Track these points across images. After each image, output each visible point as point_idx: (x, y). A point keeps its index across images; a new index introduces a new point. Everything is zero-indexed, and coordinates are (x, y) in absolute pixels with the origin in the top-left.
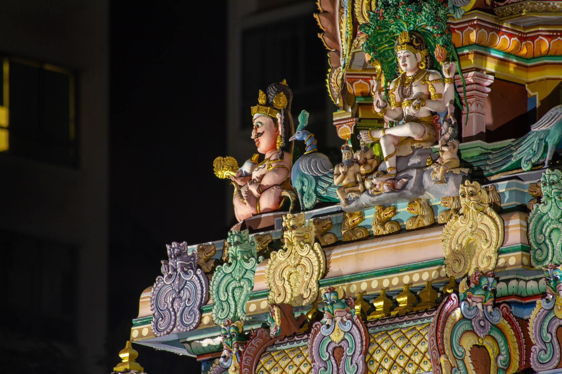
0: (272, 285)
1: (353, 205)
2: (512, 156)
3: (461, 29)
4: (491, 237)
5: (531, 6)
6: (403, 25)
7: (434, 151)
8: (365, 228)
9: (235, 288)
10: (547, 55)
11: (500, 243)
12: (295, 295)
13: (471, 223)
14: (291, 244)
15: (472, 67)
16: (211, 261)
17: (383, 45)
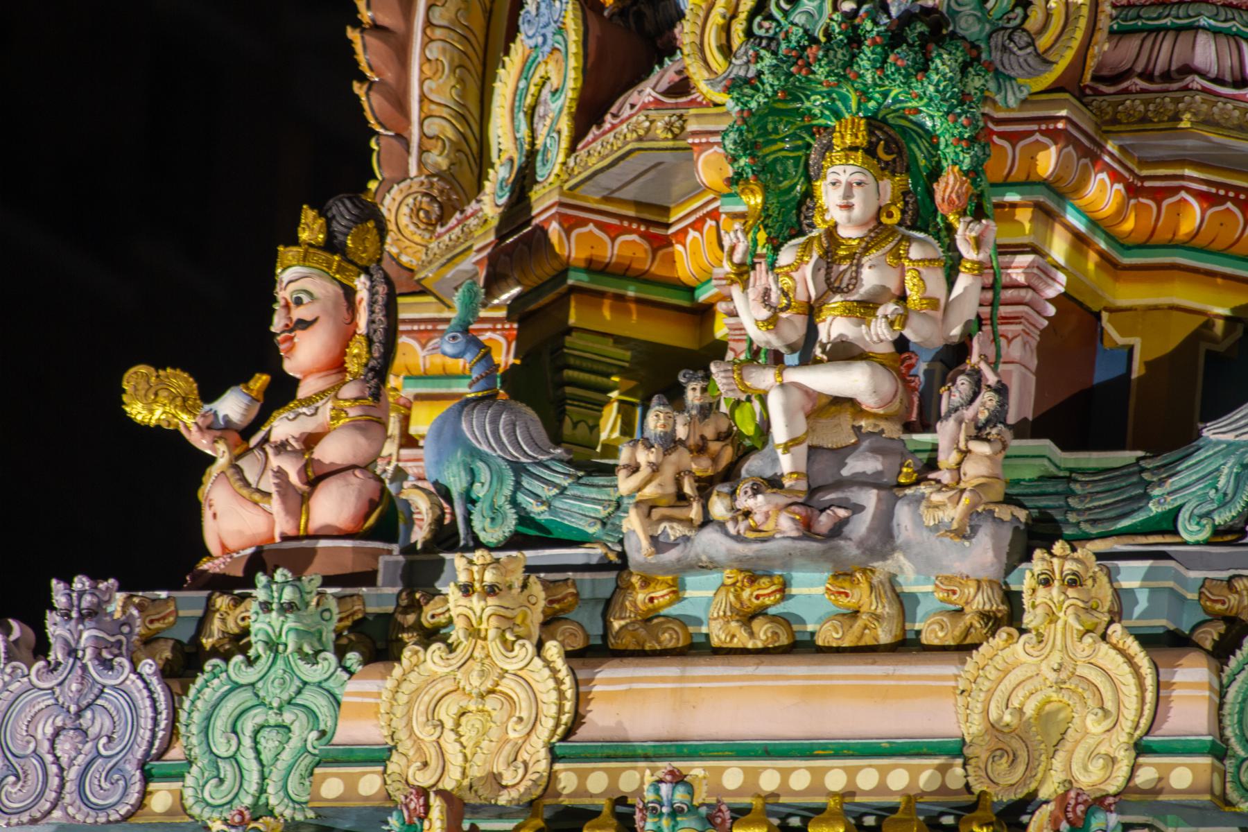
0: (402, 735)
1: (672, 555)
2: (1150, 498)
3: (1013, 138)
4: (1118, 703)
5: (1205, 107)
6: (844, 99)
7: (911, 447)
8: (683, 621)
9: (262, 727)
10: (1188, 245)
11: (1144, 723)
12: (476, 772)
13: (1055, 659)
14: (474, 633)
15: (1025, 240)
16: (162, 643)
17: (774, 142)
